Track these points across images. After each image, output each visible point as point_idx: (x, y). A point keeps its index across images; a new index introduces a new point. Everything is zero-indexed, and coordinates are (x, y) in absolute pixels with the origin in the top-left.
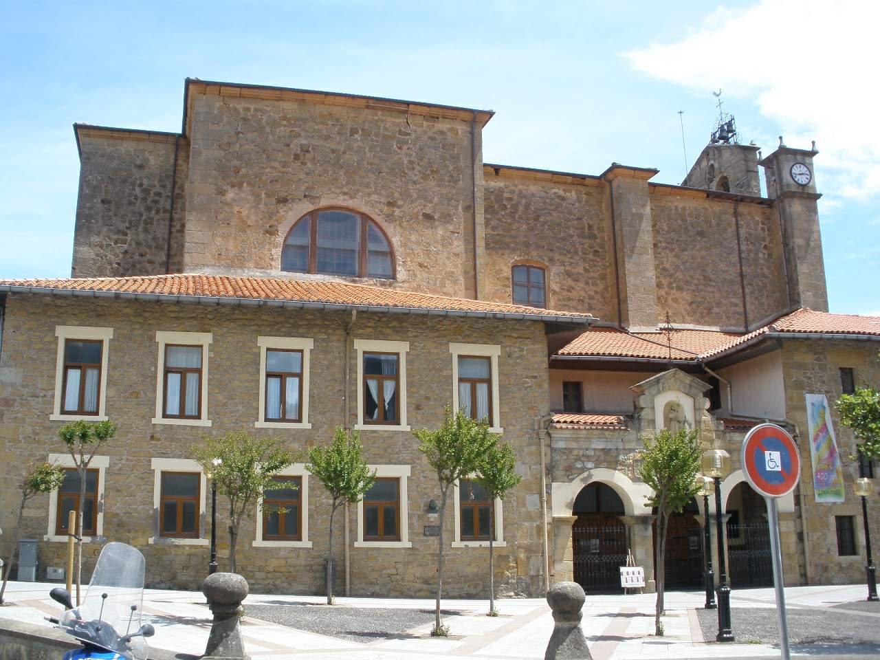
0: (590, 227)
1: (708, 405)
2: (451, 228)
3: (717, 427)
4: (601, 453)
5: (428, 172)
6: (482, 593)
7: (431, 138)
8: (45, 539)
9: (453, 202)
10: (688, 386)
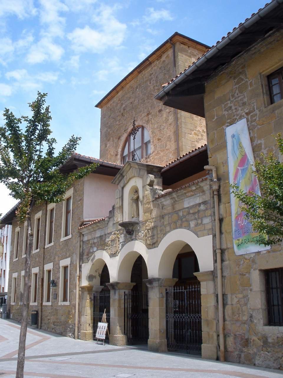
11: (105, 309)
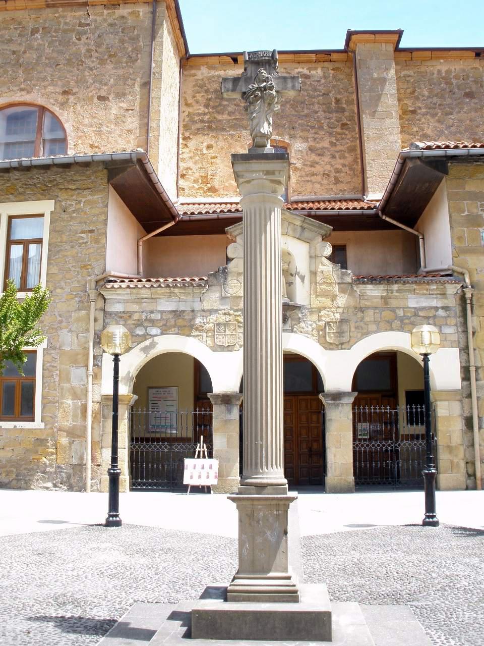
0: (338, 101)
1: (328, 250)
2: (124, 105)
3: (342, 279)
4: (170, 316)
5: (106, 57)
6: (14, 482)
7: (111, 25)
8: (136, 397)
9: (129, 82)
10: (299, 229)
11: (202, 437)
